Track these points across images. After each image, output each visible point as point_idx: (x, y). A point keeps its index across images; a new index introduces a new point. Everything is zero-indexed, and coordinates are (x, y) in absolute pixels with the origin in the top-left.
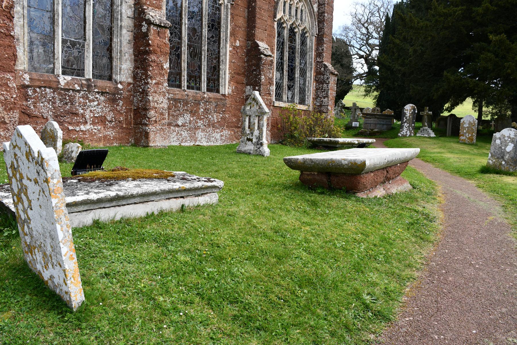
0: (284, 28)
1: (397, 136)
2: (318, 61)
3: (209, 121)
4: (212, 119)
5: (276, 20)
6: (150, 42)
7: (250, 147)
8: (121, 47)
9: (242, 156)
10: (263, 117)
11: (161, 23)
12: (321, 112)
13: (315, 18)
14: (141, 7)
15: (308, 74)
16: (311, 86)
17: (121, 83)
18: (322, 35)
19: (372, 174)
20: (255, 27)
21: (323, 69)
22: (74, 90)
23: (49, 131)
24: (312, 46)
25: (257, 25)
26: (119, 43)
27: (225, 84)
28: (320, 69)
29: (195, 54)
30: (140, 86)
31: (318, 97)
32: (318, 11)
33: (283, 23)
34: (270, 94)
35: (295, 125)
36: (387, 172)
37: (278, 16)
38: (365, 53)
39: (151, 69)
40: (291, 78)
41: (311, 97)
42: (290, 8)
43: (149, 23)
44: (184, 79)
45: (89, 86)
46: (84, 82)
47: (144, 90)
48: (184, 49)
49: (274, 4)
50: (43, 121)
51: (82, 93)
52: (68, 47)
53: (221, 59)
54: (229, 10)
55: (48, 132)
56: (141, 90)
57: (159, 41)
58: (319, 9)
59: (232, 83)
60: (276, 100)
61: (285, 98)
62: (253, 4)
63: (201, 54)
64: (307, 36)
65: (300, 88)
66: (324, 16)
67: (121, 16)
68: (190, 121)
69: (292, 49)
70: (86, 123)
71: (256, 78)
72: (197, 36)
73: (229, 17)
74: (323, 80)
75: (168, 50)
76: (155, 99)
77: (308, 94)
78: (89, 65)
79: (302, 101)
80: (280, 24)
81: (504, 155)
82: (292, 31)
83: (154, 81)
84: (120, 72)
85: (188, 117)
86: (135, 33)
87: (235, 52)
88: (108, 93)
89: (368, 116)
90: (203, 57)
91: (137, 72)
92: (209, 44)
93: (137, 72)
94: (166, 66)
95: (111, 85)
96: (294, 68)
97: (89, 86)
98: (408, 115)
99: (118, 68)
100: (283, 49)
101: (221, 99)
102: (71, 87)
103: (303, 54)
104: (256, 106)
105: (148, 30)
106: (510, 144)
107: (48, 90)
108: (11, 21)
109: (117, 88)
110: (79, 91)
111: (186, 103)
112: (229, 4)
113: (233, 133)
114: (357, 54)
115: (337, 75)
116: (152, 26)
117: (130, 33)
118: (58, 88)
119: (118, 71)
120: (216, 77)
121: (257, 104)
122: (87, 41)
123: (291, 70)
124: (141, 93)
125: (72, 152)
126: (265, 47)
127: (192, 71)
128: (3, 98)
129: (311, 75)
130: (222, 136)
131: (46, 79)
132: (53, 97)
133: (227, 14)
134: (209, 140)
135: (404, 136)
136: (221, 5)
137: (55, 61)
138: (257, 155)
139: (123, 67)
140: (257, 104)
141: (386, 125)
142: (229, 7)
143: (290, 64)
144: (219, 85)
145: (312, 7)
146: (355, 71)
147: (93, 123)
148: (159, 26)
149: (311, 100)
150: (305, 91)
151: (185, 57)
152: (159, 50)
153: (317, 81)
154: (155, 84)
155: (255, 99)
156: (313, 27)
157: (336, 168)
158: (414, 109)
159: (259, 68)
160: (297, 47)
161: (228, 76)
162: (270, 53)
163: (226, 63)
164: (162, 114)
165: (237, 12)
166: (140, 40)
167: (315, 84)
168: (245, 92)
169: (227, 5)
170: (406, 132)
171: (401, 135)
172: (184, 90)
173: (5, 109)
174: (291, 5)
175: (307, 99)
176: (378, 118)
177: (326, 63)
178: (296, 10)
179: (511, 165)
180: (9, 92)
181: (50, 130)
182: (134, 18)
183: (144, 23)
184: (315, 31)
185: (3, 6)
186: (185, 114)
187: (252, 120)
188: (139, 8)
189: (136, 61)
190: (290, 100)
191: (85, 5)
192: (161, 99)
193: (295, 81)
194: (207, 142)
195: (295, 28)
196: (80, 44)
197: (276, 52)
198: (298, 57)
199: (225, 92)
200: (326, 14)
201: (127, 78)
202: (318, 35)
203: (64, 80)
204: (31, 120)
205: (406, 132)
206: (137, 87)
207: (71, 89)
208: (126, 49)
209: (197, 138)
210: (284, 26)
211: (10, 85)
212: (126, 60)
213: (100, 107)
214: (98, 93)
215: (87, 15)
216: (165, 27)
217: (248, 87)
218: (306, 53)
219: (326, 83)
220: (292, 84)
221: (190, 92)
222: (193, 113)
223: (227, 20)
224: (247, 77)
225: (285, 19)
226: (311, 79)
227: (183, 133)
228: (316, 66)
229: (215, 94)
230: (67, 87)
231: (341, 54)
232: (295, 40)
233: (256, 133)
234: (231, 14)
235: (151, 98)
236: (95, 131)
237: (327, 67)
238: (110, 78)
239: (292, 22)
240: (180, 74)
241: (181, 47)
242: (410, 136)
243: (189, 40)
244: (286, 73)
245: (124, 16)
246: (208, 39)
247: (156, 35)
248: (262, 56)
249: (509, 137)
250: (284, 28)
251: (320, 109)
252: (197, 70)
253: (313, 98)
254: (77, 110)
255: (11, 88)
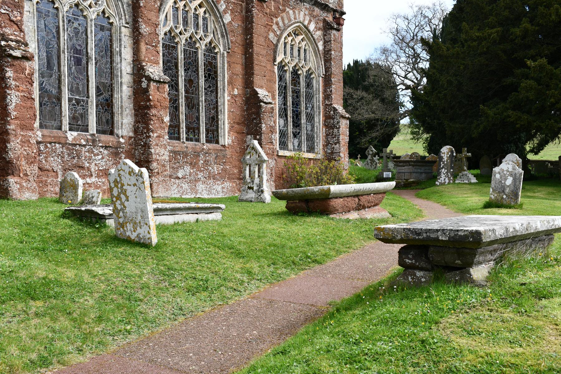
0: (286, 71)
1: (435, 185)
2: (327, 104)
3: (209, 173)
4: (212, 171)
5: (275, 63)
6: (151, 97)
7: (251, 195)
8: (121, 102)
9: (244, 204)
10: (262, 165)
11: (160, 79)
12: (330, 160)
13: (320, 57)
14: (140, 64)
15: (316, 119)
16: (320, 132)
17: (122, 137)
18: (330, 76)
19: (342, 200)
20: (253, 74)
21: (332, 112)
22: (80, 145)
23: (69, 180)
24: (319, 88)
25: (255, 72)
26: (120, 99)
27: (224, 135)
28: (330, 112)
29: (192, 105)
30: (141, 140)
31: (329, 143)
32: (324, 49)
33: (284, 66)
34: (272, 143)
35: (301, 175)
36: (359, 200)
37: (279, 59)
38: (413, 81)
39: (152, 123)
40: (297, 124)
41: (321, 144)
42: (292, 49)
43: (149, 79)
44: (183, 131)
45: (94, 141)
46: (89, 137)
47: (146, 144)
48: (182, 101)
49: (273, 47)
50: (54, 174)
51: (88, 147)
52: (73, 105)
53: (219, 108)
54: (226, 59)
55: (68, 181)
56: (142, 143)
57: (159, 95)
58: (325, 47)
59: (232, 133)
60: (281, 149)
61: (290, 146)
62: (250, 50)
63: (199, 105)
64: (313, 78)
65: (307, 134)
66: (331, 54)
67: (121, 73)
68: (190, 173)
69: (296, 94)
70: (91, 175)
71: (257, 127)
72: (194, 87)
73: (226, 65)
74: (333, 124)
75: (167, 104)
76: (157, 151)
77: (318, 141)
78: (93, 121)
79: (311, 149)
80: (281, 67)
81: (504, 189)
82: (295, 74)
83: (155, 135)
84: (122, 127)
85: (188, 169)
86: (134, 89)
87: (233, 101)
88: (111, 147)
89: (401, 164)
90: (201, 108)
91: (138, 126)
92: (206, 94)
93: (138, 126)
94: (167, 119)
95: (114, 139)
96: (300, 113)
97: (94, 141)
98: (445, 158)
99: (120, 123)
100: (285, 94)
101: (221, 150)
102: (78, 142)
103: (309, 97)
104: (255, 155)
105: (148, 85)
106: (509, 177)
107: (57, 145)
108: (32, 85)
109: (119, 142)
110: (84, 146)
111: (186, 155)
112: (225, 52)
113: (234, 185)
114: (403, 84)
115: (348, 118)
116: (152, 83)
117: (130, 89)
118: (66, 143)
119: (120, 125)
120: (214, 128)
121: (256, 152)
122: (91, 98)
123: (297, 116)
124: (143, 146)
125: (93, 197)
126: (265, 94)
127: (190, 122)
128: (26, 153)
129: (319, 120)
130: (223, 188)
131: (56, 135)
132: (62, 152)
133: (224, 62)
134: (210, 192)
135: (441, 184)
136: (216, 53)
137: (63, 118)
138: (259, 202)
139: (124, 121)
140: (256, 152)
141: (425, 173)
142: (226, 55)
143: (295, 109)
144: (218, 136)
145: (317, 46)
146: (403, 106)
147: (98, 176)
148: (158, 82)
149: (321, 147)
150: (314, 138)
151: (183, 109)
152: (159, 104)
153: (326, 126)
154: (157, 137)
155: (253, 148)
156: (319, 67)
157: (311, 195)
158: (452, 152)
159: (259, 116)
160: (302, 90)
161: (227, 126)
162: (270, 100)
163: (224, 113)
164: (164, 166)
165: (233, 60)
166: (141, 97)
167: (324, 129)
168: (245, 142)
169: (223, 54)
170: (445, 179)
171: (438, 183)
172: (183, 142)
173: (27, 163)
174: (293, 45)
175: (316, 147)
176: (413, 166)
177: (335, 106)
178: (299, 51)
179: (511, 198)
180: (31, 147)
181: (71, 179)
182: (133, 74)
183: (144, 79)
184: (322, 71)
185: (26, 74)
186: (185, 167)
187: (252, 168)
188: (138, 65)
189: (136, 115)
190: (296, 148)
191: (87, 64)
192: (162, 151)
193: (301, 127)
194: (208, 195)
195: (298, 70)
196: (83, 101)
197: (277, 97)
198: (303, 101)
199: (225, 142)
200: (333, 52)
201: (128, 132)
202: (325, 75)
203: (71, 136)
204: (43, 173)
205: (445, 179)
206: (139, 140)
207: (78, 144)
208: (127, 104)
209: (197, 190)
210: (285, 69)
211: (32, 142)
212: (127, 115)
213: (104, 160)
214: (102, 147)
215: (89, 73)
216: (164, 83)
217: (249, 136)
218: (313, 96)
219: (337, 128)
220: (298, 131)
221: (189, 144)
222: (193, 165)
223: (223, 68)
224: (248, 126)
225: (287, 61)
226: (320, 124)
227: (184, 185)
228: (325, 110)
229: (214, 145)
230: (74, 142)
231: (381, 85)
232: (299, 83)
233: (257, 180)
234: (228, 62)
235: (153, 151)
236: (100, 184)
237: (337, 110)
238: (112, 133)
239: (295, 64)
240: (178, 126)
241: (179, 99)
242: (449, 183)
243: (187, 91)
244: (290, 119)
245: (124, 73)
246: (205, 89)
247: (156, 91)
248: (262, 104)
249: (508, 171)
250: (286, 71)
251: (331, 156)
252: (195, 121)
253: (323, 145)
254: (83, 163)
255: (32, 144)
